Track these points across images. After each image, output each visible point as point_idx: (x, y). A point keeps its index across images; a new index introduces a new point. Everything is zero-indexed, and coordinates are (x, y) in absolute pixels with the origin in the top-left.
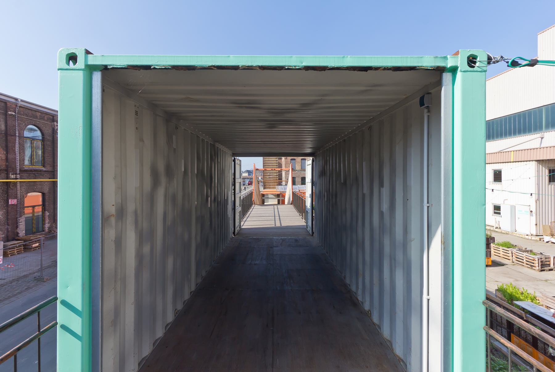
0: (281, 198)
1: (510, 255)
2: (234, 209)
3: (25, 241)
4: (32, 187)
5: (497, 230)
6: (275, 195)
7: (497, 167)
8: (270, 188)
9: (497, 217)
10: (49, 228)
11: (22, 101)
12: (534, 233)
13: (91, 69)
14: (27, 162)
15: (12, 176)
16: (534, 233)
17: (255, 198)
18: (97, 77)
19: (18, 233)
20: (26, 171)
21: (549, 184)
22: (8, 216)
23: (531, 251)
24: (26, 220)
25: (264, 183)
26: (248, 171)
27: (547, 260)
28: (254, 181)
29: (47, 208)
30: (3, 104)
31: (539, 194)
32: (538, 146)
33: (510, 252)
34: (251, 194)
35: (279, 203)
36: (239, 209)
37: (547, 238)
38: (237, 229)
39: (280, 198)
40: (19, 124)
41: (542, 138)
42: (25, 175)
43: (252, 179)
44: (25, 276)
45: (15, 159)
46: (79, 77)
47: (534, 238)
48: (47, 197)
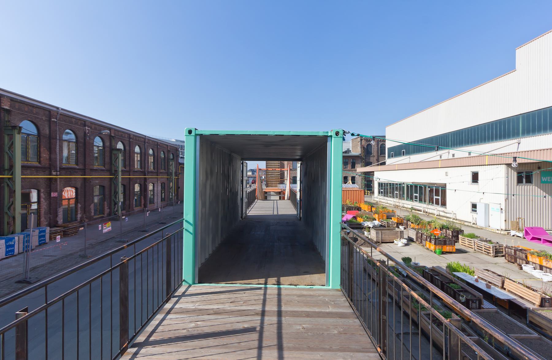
0: (282, 196)
1: (473, 244)
2: (242, 199)
3: (64, 227)
4: (68, 183)
5: (473, 225)
6: (276, 193)
7: (475, 169)
8: (272, 186)
9: (474, 214)
10: (81, 218)
11: (62, 109)
12: (504, 228)
13: (196, 135)
14: (64, 161)
15: (54, 173)
16: (504, 228)
17: (258, 193)
18: (198, 138)
19: (57, 222)
20: (64, 169)
21: (517, 185)
22: (50, 206)
23: (490, 241)
24: (63, 211)
25: (267, 181)
26: (252, 170)
27: (501, 248)
28: (257, 179)
29: (79, 201)
30: (47, 113)
31: (508, 194)
32: (516, 151)
33: (473, 242)
34: (255, 190)
35: (280, 199)
36: (245, 200)
37: (513, 233)
38: (244, 215)
39: (281, 194)
40: (59, 129)
41: (519, 143)
42: (64, 172)
43: (255, 178)
44: (71, 254)
45: (56, 158)
46: (193, 138)
47: (502, 232)
48: (79, 191)
